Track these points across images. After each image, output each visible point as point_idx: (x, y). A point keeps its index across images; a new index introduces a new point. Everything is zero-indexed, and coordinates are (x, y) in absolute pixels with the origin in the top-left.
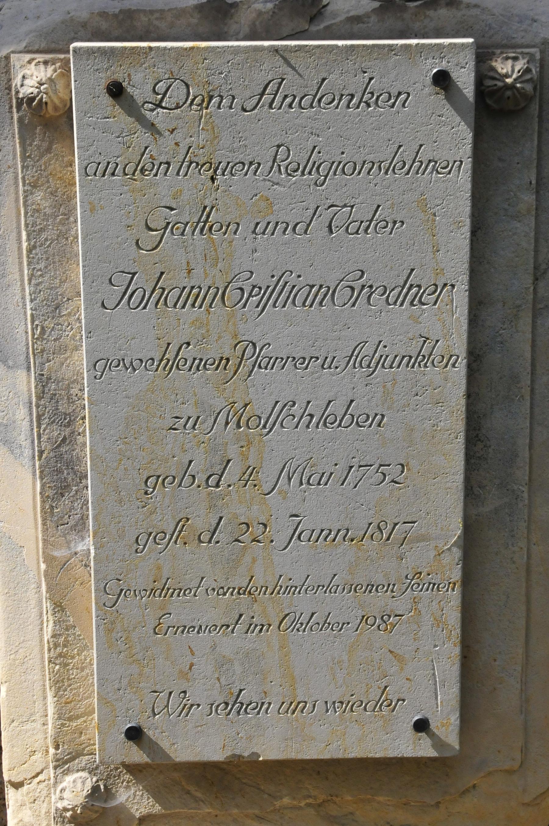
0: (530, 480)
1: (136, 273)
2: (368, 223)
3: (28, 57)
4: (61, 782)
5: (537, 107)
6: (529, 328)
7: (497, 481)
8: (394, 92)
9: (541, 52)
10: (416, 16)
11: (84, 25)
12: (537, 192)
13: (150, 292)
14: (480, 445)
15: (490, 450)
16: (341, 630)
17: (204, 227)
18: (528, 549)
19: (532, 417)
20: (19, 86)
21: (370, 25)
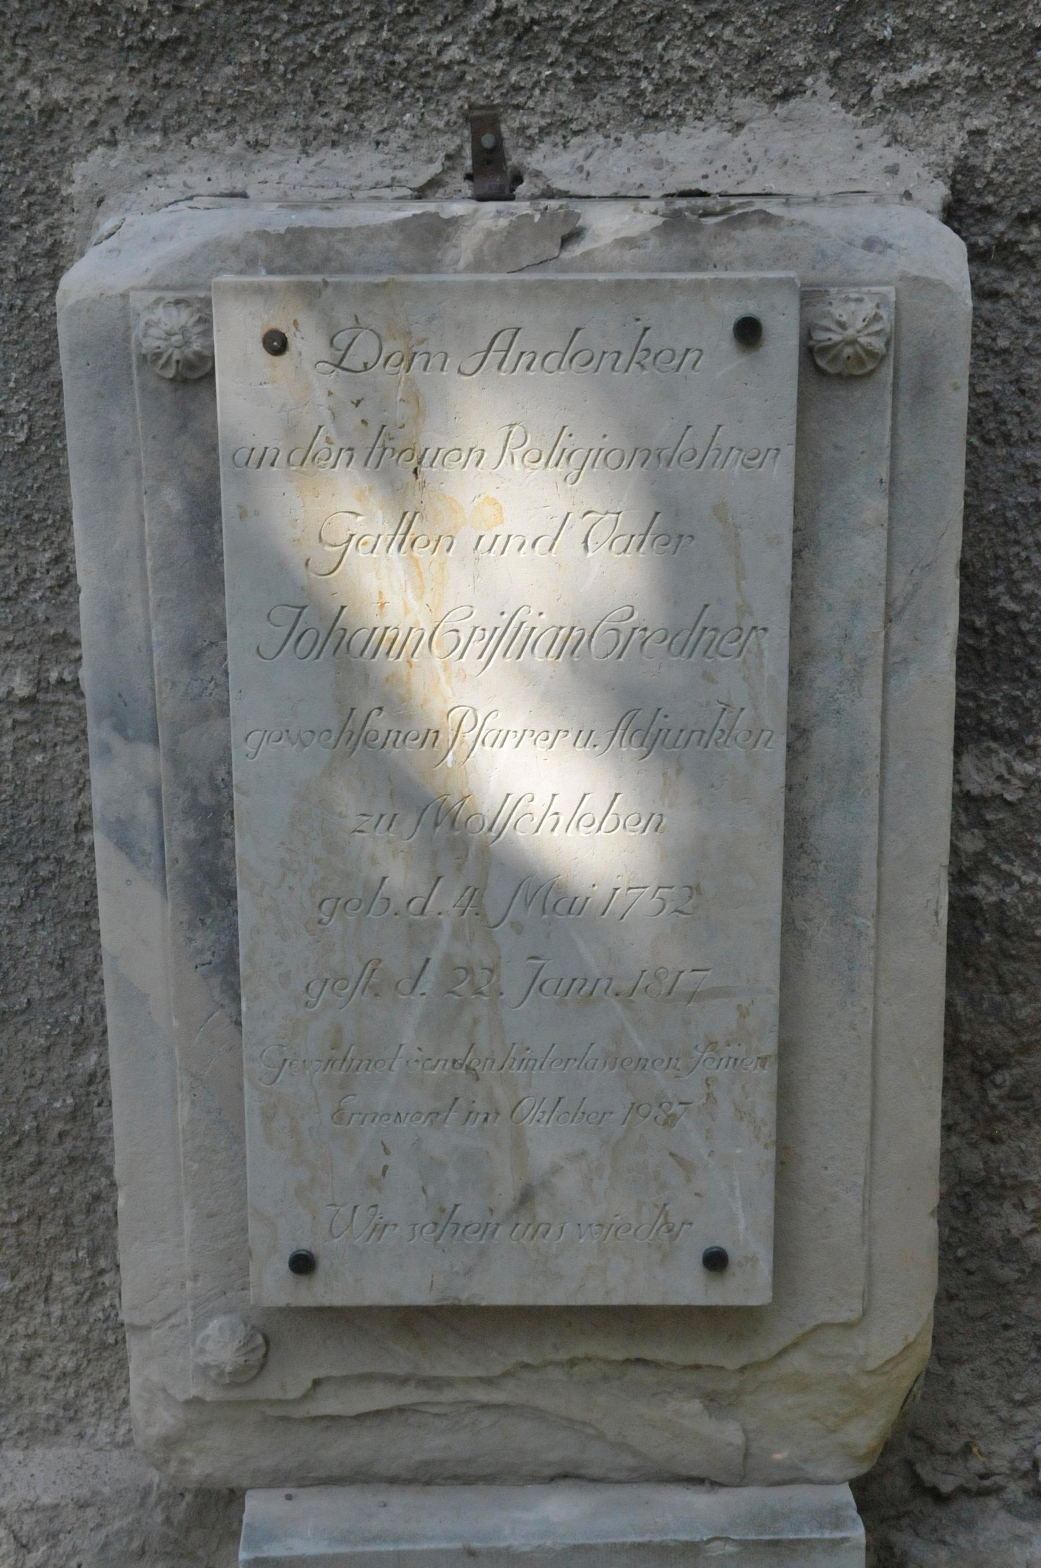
0: (878, 910)
1: (306, 607)
2: (641, 537)
3: (155, 295)
4: (703, 88)
5: (891, 370)
6: (878, 691)
7: (830, 912)
8: (680, 350)
9: (897, 291)
10: (715, 237)
11: (236, 250)
12: (891, 494)
13: (325, 636)
14: (805, 860)
15: (821, 867)
16: (600, 1122)
17: (403, 540)
18: (875, 1010)
19: (881, 820)
20: (140, 336)
21: (648, 250)
